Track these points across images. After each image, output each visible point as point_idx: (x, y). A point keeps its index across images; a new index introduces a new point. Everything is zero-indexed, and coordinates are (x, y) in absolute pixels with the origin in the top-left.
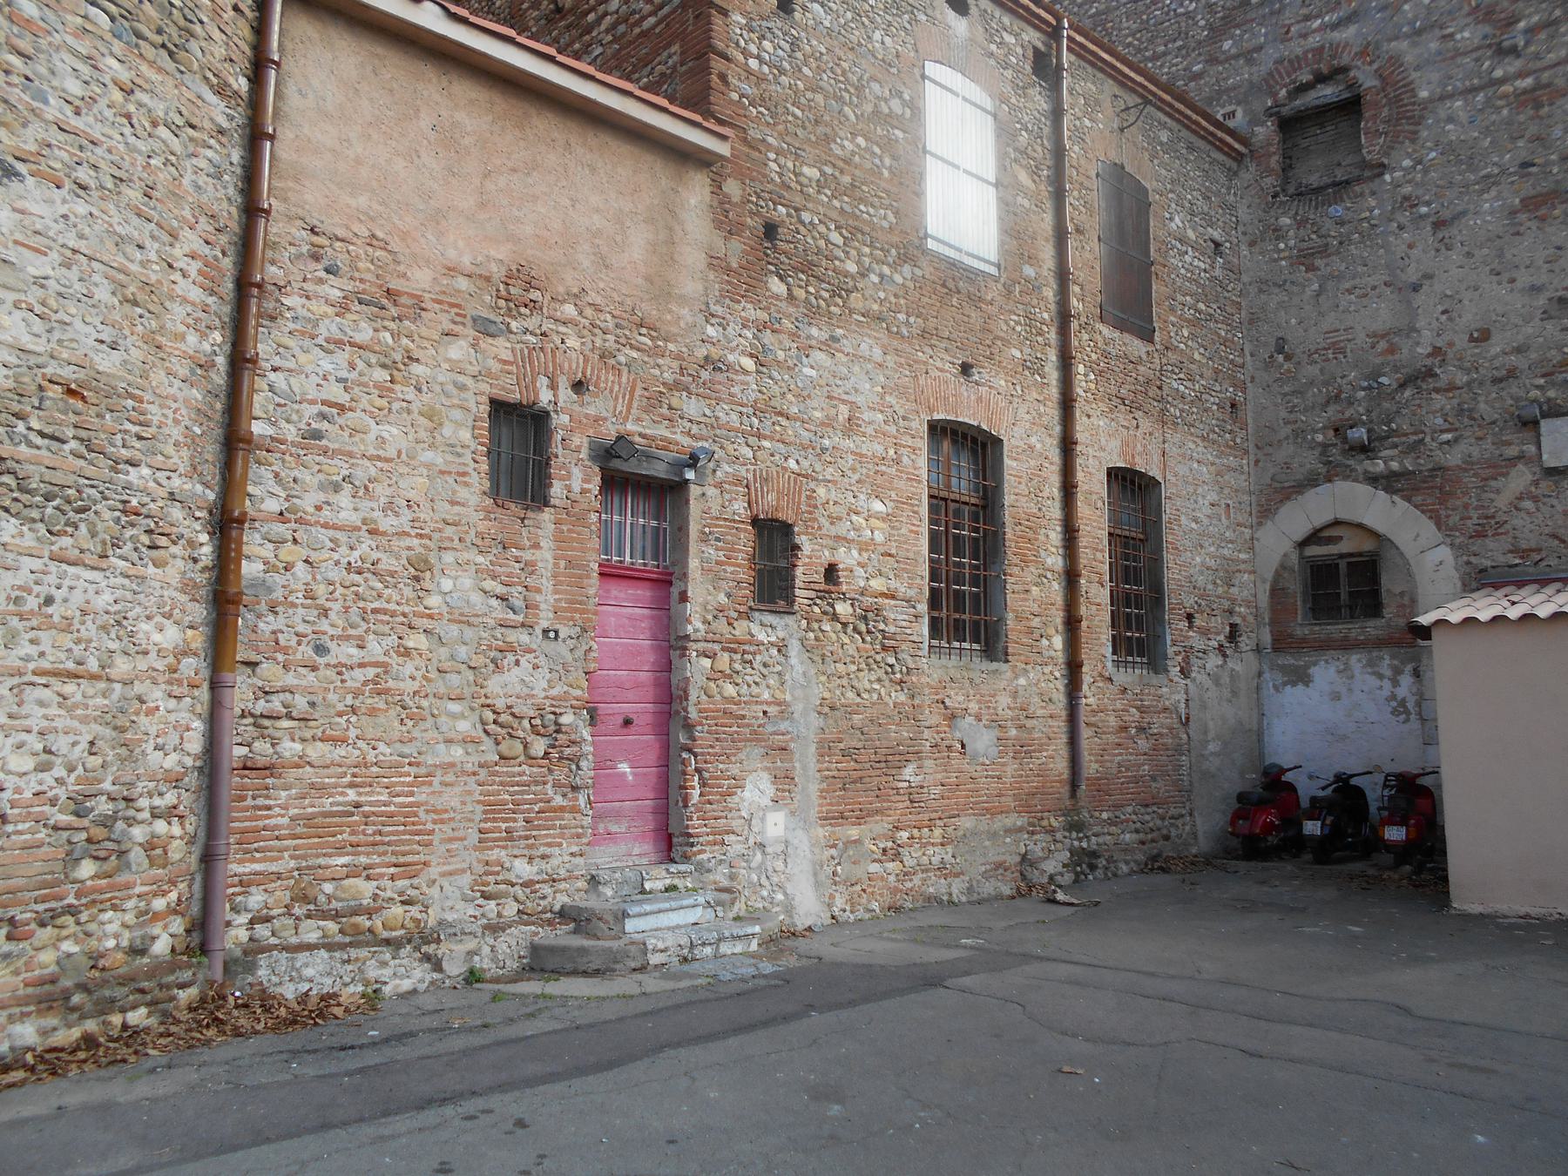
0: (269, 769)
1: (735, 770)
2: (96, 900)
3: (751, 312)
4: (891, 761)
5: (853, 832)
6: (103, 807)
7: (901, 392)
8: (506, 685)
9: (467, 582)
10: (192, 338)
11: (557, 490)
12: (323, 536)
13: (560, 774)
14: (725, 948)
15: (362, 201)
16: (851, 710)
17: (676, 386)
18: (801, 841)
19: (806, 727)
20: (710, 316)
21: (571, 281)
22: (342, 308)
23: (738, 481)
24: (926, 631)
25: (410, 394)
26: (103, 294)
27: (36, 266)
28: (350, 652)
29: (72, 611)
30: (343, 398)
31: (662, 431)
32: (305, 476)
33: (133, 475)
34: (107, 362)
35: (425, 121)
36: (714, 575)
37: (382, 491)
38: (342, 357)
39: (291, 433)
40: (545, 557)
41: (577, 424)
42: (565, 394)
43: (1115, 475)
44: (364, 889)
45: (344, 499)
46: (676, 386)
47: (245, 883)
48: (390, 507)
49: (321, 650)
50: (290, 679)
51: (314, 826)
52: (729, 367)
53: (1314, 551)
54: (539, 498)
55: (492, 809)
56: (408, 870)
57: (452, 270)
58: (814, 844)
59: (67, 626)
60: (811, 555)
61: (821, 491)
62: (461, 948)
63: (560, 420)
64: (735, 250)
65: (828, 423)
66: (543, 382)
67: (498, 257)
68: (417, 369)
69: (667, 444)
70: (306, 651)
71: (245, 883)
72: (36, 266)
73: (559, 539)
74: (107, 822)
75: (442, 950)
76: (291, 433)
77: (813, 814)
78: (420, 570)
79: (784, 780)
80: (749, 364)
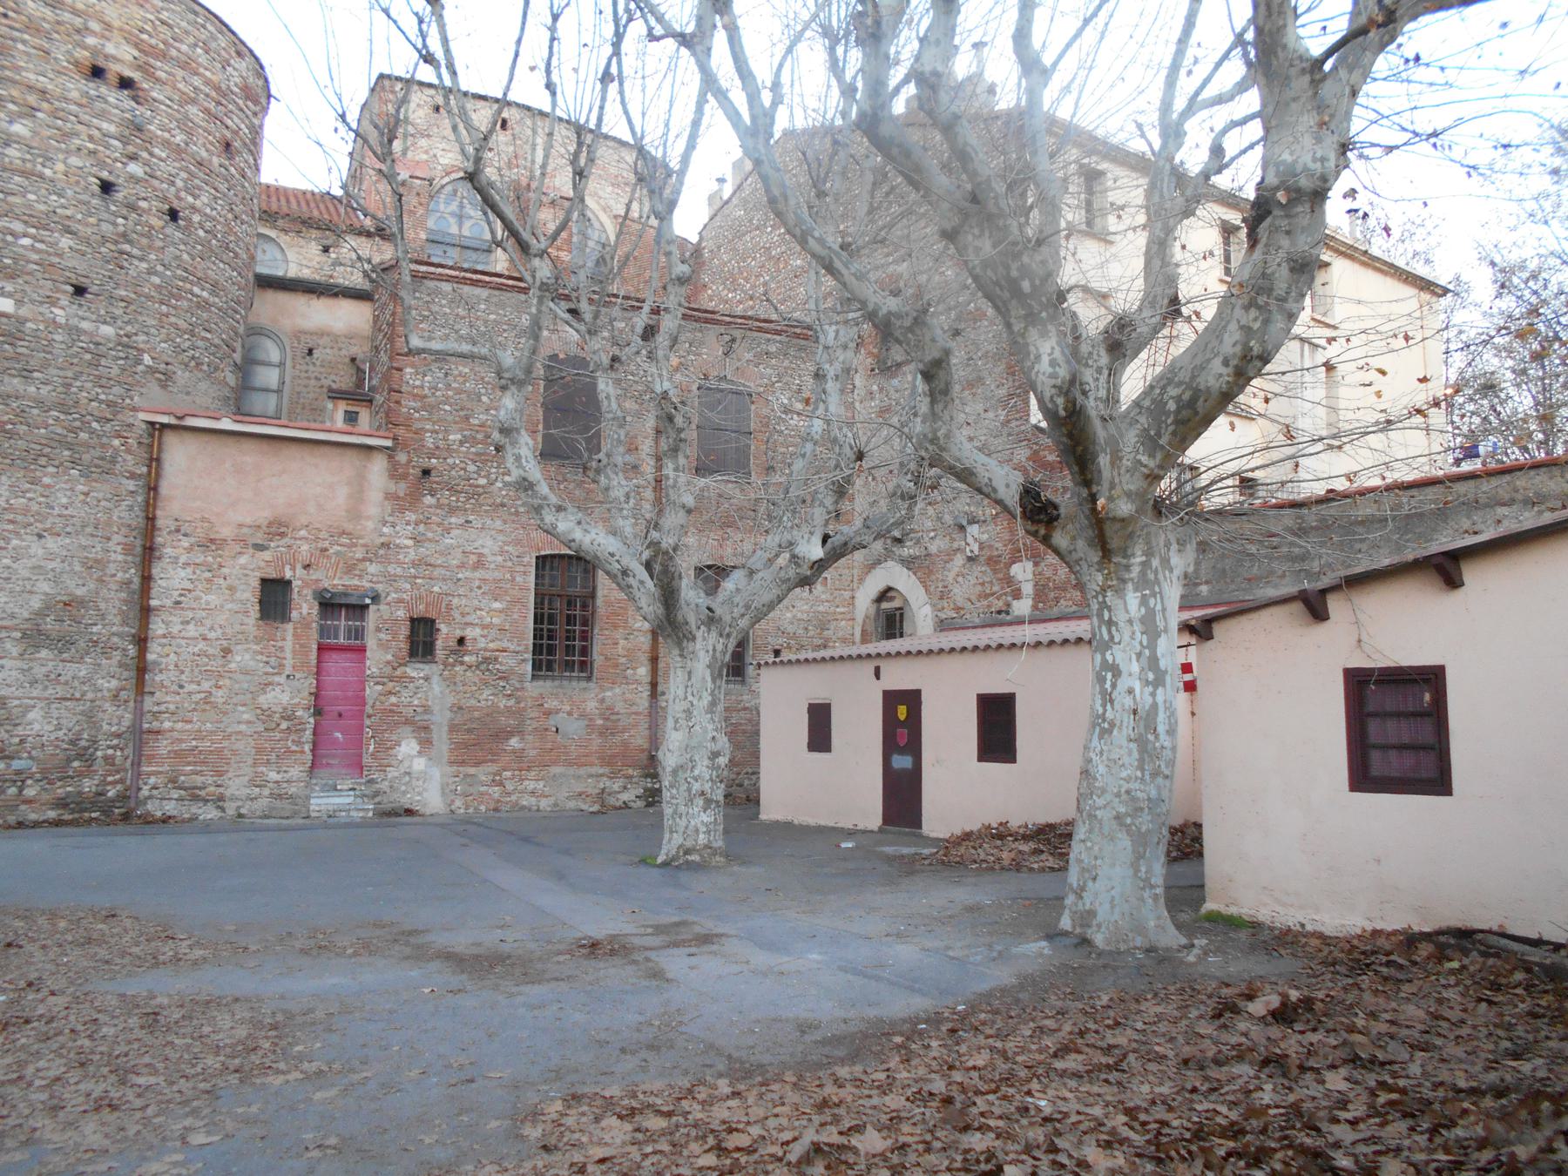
0: (158, 732)
1: (394, 737)
2: (80, 775)
3: (413, 517)
4: (503, 735)
5: (472, 771)
6: (83, 743)
7: (517, 542)
8: (267, 699)
9: (247, 657)
10: (120, 575)
11: (294, 615)
12: (183, 642)
13: (293, 737)
14: (354, 814)
15: (198, 503)
16: (472, 709)
17: (364, 560)
18: (436, 773)
19: (440, 719)
20: (385, 523)
21: (304, 520)
22: (189, 550)
23: (401, 601)
24: (529, 667)
25: (221, 581)
26: (78, 568)
27: (51, 565)
28: (193, 687)
29: (69, 677)
30: (191, 587)
31: (356, 582)
32: (172, 618)
33: (95, 629)
34: (80, 592)
35: (228, 465)
36: (383, 646)
37: (208, 623)
38: (189, 570)
39: (168, 603)
40: (289, 645)
41: (306, 584)
42: (300, 571)
43: (699, 570)
44: (199, 780)
45: (191, 627)
46: (364, 560)
47: (150, 774)
48: (212, 628)
49: (181, 687)
50: (168, 698)
51: (178, 754)
52: (398, 546)
53: (885, 605)
54: (284, 617)
55: (259, 751)
56: (220, 774)
57: (240, 526)
58: (442, 776)
59: (66, 683)
60: (446, 633)
61: (455, 601)
62: (234, 805)
63: (296, 584)
64: (402, 488)
65: (462, 566)
66: (287, 568)
67: (263, 515)
68: (225, 570)
69: (357, 588)
70: (175, 688)
71: (150, 774)
72: (51, 565)
73: (295, 635)
74: (86, 749)
75: (226, 805)
76: (168, 603)
77: (445, 760)
78: (226, 651)
79: (426, 743)
80: (410, 543)
